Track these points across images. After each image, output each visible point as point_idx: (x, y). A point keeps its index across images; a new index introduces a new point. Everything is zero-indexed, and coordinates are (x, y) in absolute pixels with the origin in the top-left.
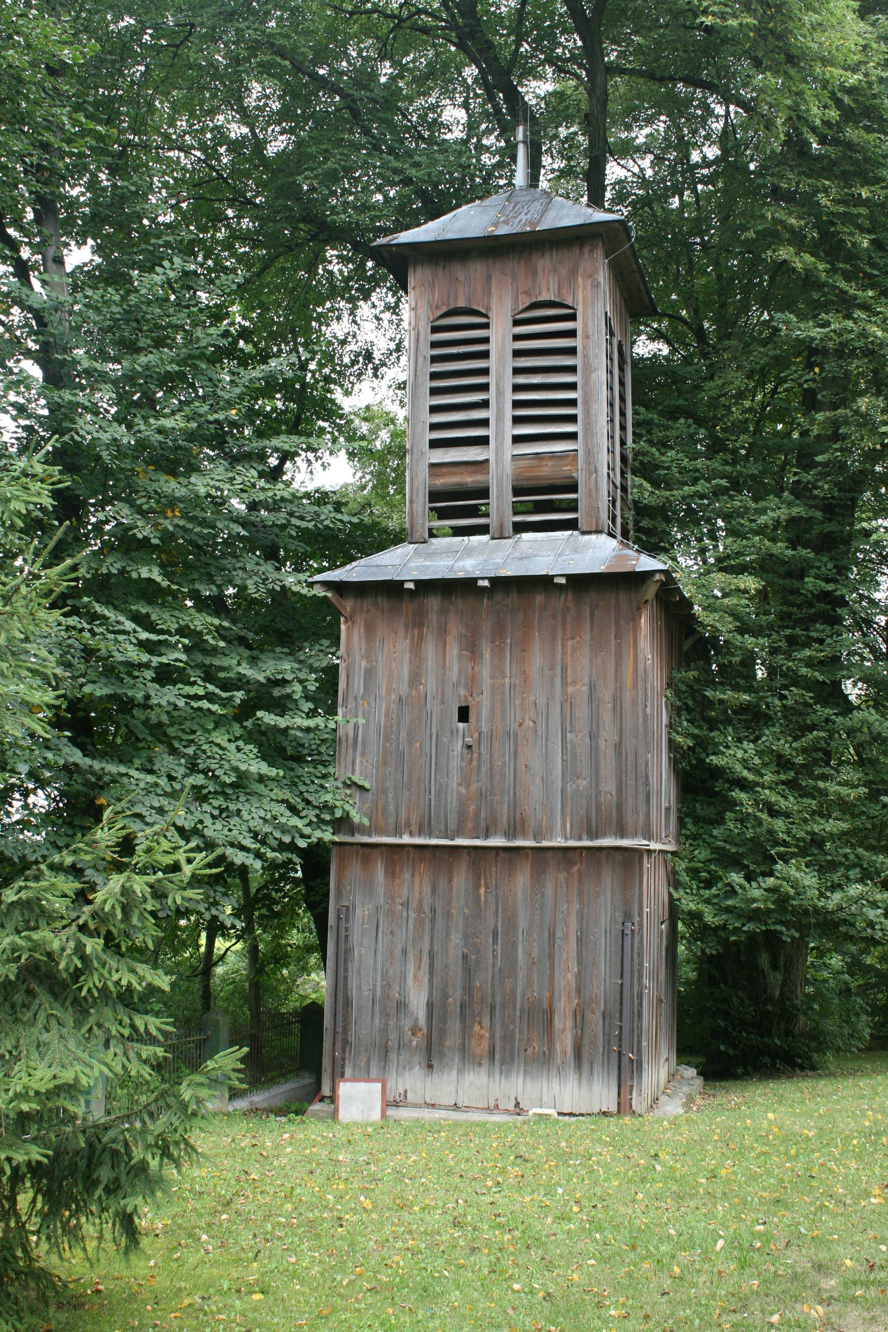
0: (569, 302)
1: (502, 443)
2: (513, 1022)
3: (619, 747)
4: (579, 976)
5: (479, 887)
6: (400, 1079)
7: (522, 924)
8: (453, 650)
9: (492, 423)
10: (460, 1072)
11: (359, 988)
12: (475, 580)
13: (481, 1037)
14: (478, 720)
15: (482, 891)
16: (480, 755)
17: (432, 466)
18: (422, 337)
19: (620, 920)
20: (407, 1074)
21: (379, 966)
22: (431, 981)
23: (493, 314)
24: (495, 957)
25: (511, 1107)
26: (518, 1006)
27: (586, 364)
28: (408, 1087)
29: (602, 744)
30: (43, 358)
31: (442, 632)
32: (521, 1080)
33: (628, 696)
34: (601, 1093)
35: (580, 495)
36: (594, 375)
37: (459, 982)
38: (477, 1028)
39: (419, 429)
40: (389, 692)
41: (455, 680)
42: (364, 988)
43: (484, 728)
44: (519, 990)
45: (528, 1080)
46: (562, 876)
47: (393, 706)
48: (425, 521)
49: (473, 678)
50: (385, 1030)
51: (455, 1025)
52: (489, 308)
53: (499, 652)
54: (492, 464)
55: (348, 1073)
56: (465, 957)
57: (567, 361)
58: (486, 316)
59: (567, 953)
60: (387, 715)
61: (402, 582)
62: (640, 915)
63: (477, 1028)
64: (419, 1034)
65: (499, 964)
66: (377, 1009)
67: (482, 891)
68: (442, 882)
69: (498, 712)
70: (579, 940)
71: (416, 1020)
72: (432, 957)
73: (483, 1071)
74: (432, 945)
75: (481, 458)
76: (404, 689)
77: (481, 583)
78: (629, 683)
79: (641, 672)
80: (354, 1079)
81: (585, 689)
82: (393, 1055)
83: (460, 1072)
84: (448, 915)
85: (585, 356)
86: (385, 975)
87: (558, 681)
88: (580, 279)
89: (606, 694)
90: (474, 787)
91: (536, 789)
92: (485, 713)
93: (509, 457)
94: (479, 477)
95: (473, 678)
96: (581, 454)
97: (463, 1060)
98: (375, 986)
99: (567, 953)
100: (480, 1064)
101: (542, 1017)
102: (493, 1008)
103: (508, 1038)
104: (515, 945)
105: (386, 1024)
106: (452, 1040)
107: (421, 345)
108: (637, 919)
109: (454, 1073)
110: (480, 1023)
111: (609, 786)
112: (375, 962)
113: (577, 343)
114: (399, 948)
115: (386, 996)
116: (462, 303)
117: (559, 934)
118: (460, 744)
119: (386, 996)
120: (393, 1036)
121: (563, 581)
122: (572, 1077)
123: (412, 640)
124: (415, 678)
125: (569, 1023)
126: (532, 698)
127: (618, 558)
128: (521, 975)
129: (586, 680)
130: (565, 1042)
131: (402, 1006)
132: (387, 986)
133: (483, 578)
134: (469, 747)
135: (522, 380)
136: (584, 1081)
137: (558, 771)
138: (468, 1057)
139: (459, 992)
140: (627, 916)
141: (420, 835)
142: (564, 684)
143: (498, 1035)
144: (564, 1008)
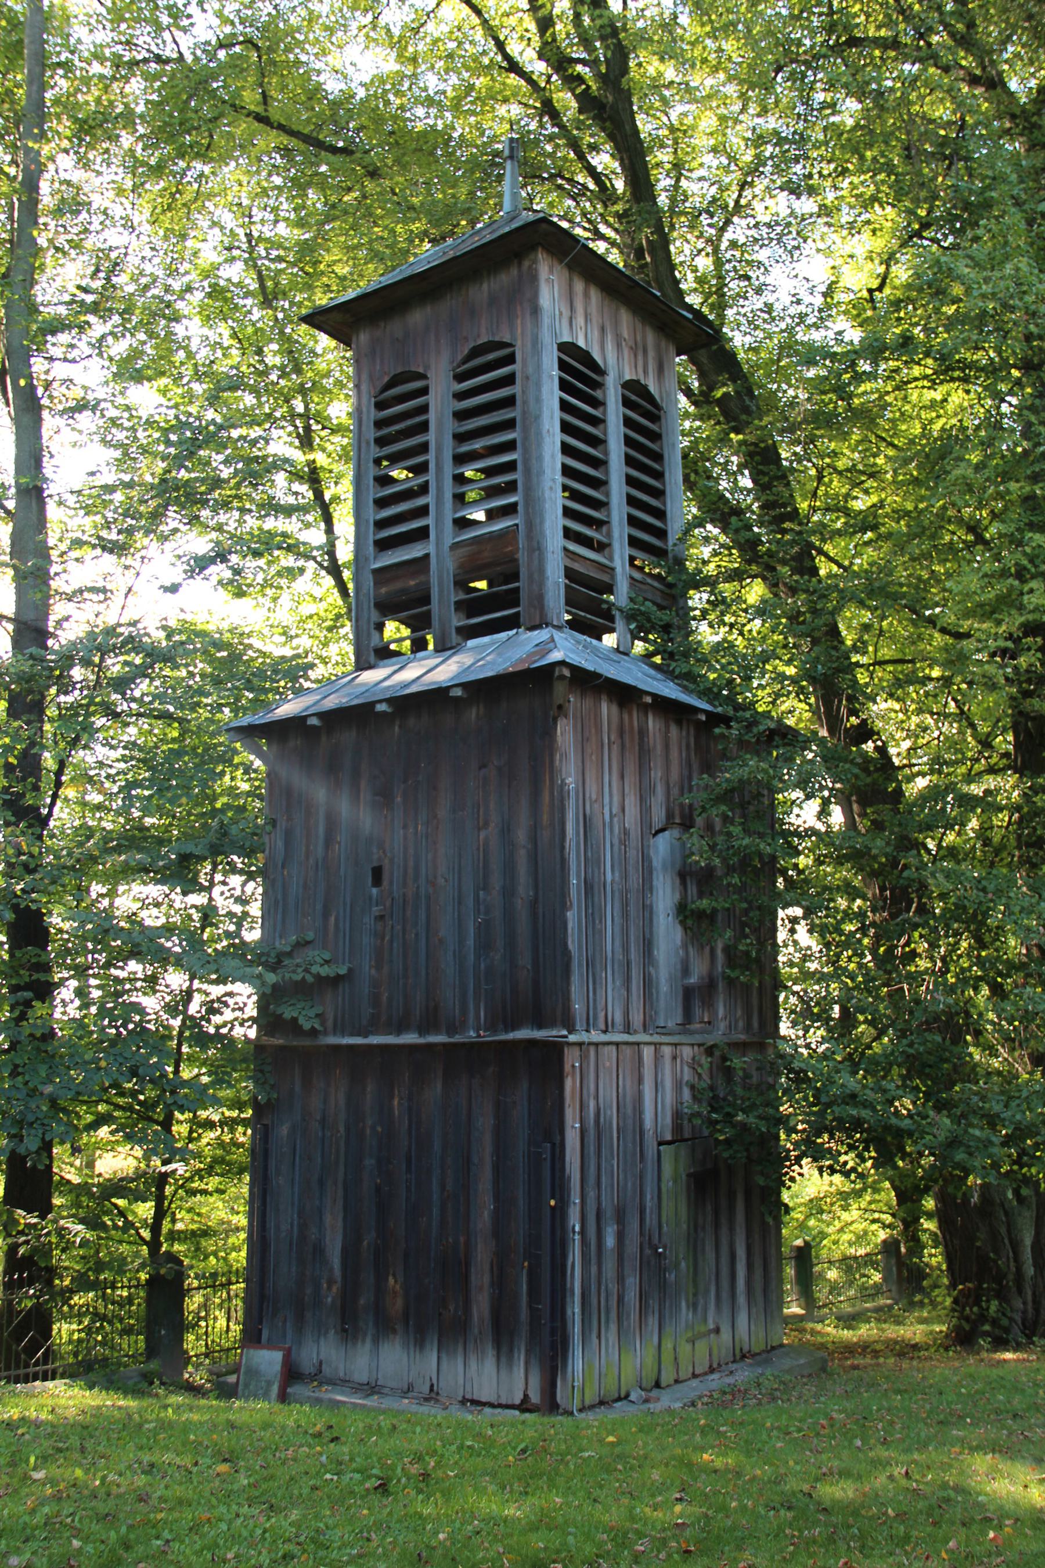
0: (507, 339)
5: (392, 1097)
9: (432, 509)
10: (376, 1341)
17: (376, 572)
25: (426, 1389)
28: (322, 1356)
30: (217, 763)
34: (520, 1379)
35: (522, 584)
48: (459, 639)
52: (427, 367)
54: (433, 560)
56: (378, 1189)
67: (396, 1102)
68: (503, 1373)
70: (496, 1169)
71: (331, 1270)
76: (320, 851)
77: (381, 707)
83: (376, 1341)
89: (521, 836)
100: (394, 1331)
101: (456, 1270)
111: (525, 960)
113: (517, 389)
125: (486, 1279)
128: (435, 1211)
130: (481, 1306)
131: (319, 1251)
133: (380, 701)
136: (503, 1359)
137: (470, 942)
144: (483, 1254)
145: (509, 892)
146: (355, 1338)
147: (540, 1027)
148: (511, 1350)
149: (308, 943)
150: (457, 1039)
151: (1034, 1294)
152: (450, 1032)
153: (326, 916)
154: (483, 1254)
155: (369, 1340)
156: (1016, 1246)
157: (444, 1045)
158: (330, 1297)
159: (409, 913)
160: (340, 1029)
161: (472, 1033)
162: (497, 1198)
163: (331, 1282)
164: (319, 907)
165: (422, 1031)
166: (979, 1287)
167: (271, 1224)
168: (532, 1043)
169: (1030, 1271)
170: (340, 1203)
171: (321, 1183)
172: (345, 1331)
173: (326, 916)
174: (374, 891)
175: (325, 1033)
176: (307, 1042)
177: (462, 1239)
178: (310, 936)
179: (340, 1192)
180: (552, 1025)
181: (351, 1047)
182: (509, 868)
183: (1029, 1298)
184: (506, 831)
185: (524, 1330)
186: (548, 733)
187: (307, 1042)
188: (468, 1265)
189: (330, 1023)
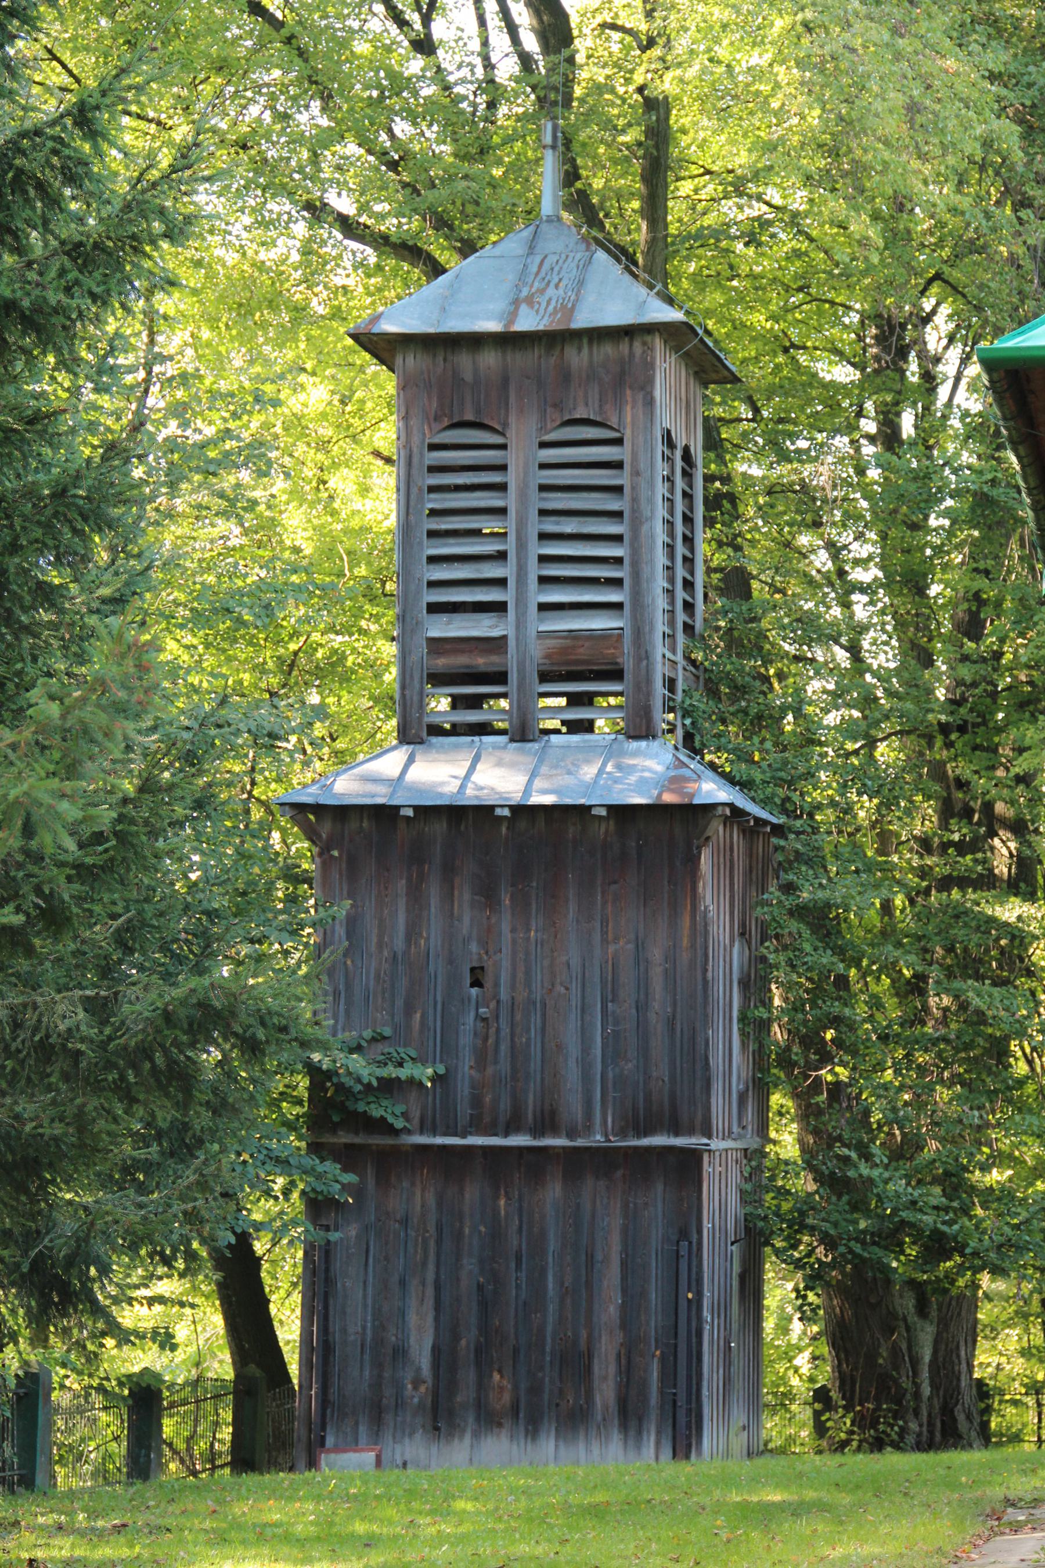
0: (613, 422)
1: (525, 613)
2: (542, 1368)
3: (671, 1022)
4: (624, 1308)
6: (398, 1448)
7: (552, 1245)
8: (464, 895)
9: (511, 583)
11: (344, 1331)
12: (492, 808)
13: (501, 1389)
14: (497, 985)
15: (502, 1202)
16: (498, 1030)
17: (432, 641)
18: (415, 460)
19: (675, 1238)
20: (407, 1440)
21: (370, 1301)
22: (437, 1319)
23: (512, 433)
24: (518, 1287)
26: (548, 1349)
27: (635, 511)
29: (652, 1017)
31: (449, 871)
32: (552, 1443)
33: (685, 957)
36: (645, 528)
37: (473, 1320)
38: (496, 1377)
39: (413, 587)
40: (380, 945)
41: (465, 932)
42: (351, 1330)
43: (504, 995)
44: (549, 1329)
45: (561, 1444)
46: (602, 1184)
47: (385, 966)
49: (489, 930)
50: (946, 348)
51: (468, 1376)
52: (506, 425)
53: (522, 905)
54: (512, 643)
55: (330, 1441)
56: (480, 1287)
57: (612, 504)
58: (503, 434)
59: (611, 1279)
60: (378, 976)
61: (397, 808)
62: (700, 1232)
63: (496, 1377)
64: (422, 1389)
65: (523, 1295)
66: (367, 1357)
67: (502, 1202)
69: (520, 975)
70: (624, 1264)
71: (419, 1370)
72: (438, 1287)
73: (504, 1434)
74: (437, 1273)
75: (496, 633)
76: (399, 944)
78: (685, 942)
79: (700, 927)
80: (337, 1449)
81: (631, 946)
82: (389, 1418)
84: (458, 1236)
85: (635, 500)
86: (377, 1314)
87: (597, 937)
88: (628, 392)
90: (490, 1070)
91: (572, 1074)
92: (504, 977)
93: (534, 634)
94: (495, 659)
95: (489, 930)
96: (627, 633)
97: (478, 1419)
98: (364, 1328)
99: (611, 1279)
100: (500, 1425)
101: (576, 1363)
102: (516, 1350)
103: (535, 1390)
104: (543, 1271)
105: (380, 1376)
106: (466, 1394)
107: (415, 472)
108: (695, 1238)
109: (468, 1436)
110: (500, 1371)
111: (661, 1071)
112: (365, 1296)
114: (396, 1278)
115: (379, 1342)
116: (469, 417)
117: (599, 1256)
118: (472, 1014)
119: (379, 1342)
120: (388, 1392)
121: (603, 812)
122: (616, 1437)
123: (409, 880)
124: (412, 933)
125: (612, 1369)
126: (564, 959)
127: (675, 782)
128: (552, 1308)
129: (632, 936)
130: (605, 1392)
131: (400, 1353)
132: (380, 1327)
134: (485, 1020)
135: (551, 526)
137: (598, 1052)
138: (489, 1420)
139: (474, 1332)
140: (684, 1234)
141: (421, 1133)
142: (605, 941)
143: (523, 1386)
144: (607, 1350)
145: (642, 1007)
146: (450, 1435)
147: (677, 1134)
148: (639, 1432)
149: (385, 1038)
150: (580, 1142)
151: (929, 1415)
152: (571, 1136)
153: (409, 1010)
154: (607, 1350)
155: (468, 1436)
156: (915, 1362)
157: (564, 1148)
158: (414, 1396)
159: (518, 1017)
160: (427, 1126)
161: (598, 1137)
162: (624, 1291)
163: (417, 1382)
164: (400, 1002)
165: (537, 1131)
166: (878, 1408)
167: (335, 1327)
168: (671, 1149)
169: (926, 1390)
170: (430, 1302)
171: (403, 1283)
172: (437, 1429)
173: (409, 1010)
174: (474, 991)
175: (409, 1132)
176: (389, 1141)
177: (584, 1334)
178: (387, 1031)
179: (430, 1292)
180: (691, 1132)
181: (444, 1147)
182: (643, 984)
183: (925, 1420)
184: (640, 946)
185: (653, 1415)
186: (692, 861)
187: (389, 1141)
188: (590, 1357)
189: (416, 1121)
